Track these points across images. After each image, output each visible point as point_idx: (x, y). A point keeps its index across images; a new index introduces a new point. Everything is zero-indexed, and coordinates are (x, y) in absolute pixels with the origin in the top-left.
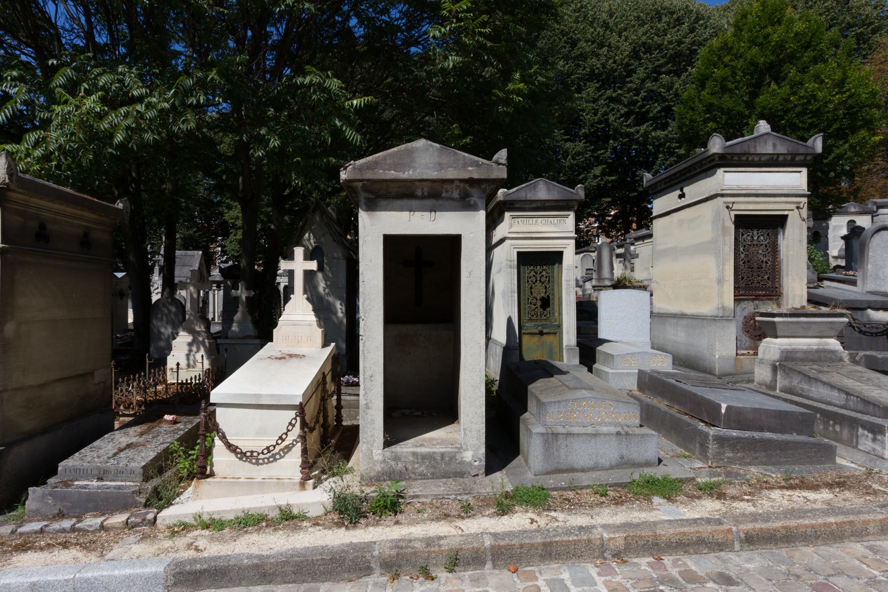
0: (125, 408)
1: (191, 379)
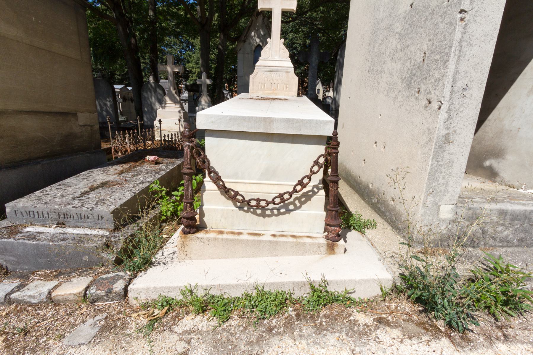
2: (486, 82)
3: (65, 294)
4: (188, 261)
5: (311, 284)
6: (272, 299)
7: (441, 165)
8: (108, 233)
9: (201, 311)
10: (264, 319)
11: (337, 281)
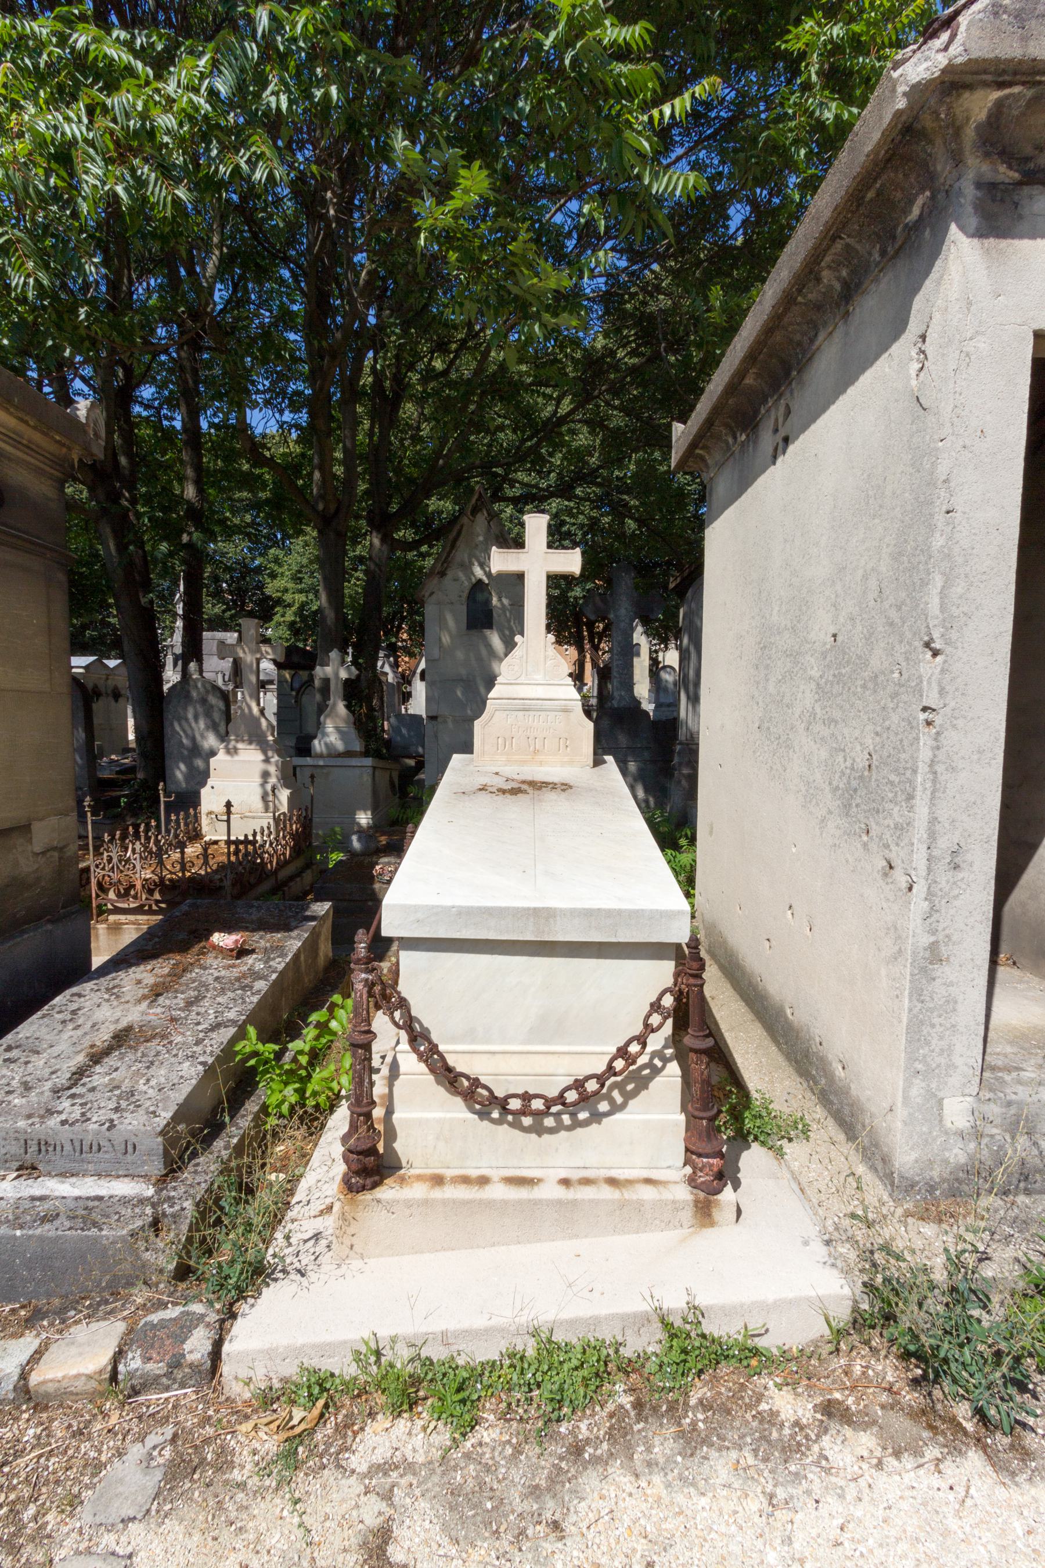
0: (119, 895)
1: (255, 834)
2: (996, 837)
3: (64, 1377)
4: (356, 1263)
5: (663, 1320)
6: (575, 1363)
7: (931, 1010)
8: (150, 1192)
9: (405, 1407)
10: (558, 1420)
11: (723, 1308)
